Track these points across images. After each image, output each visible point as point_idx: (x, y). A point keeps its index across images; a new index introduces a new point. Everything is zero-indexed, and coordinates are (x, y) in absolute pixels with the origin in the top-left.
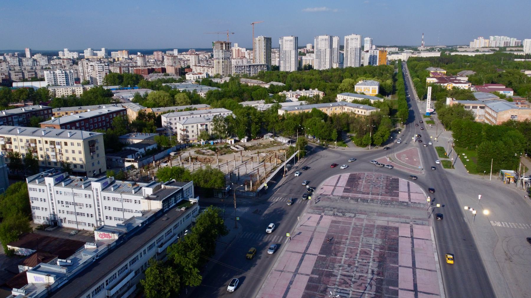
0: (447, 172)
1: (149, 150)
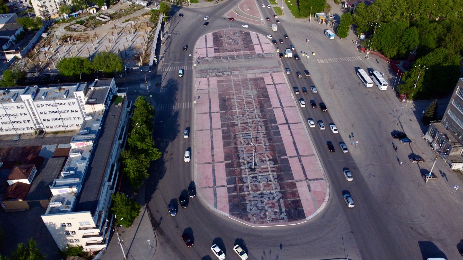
1: (18, 34)
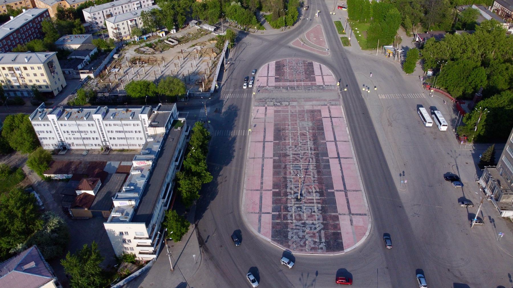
0: (346, 51)
1: (92, 55)
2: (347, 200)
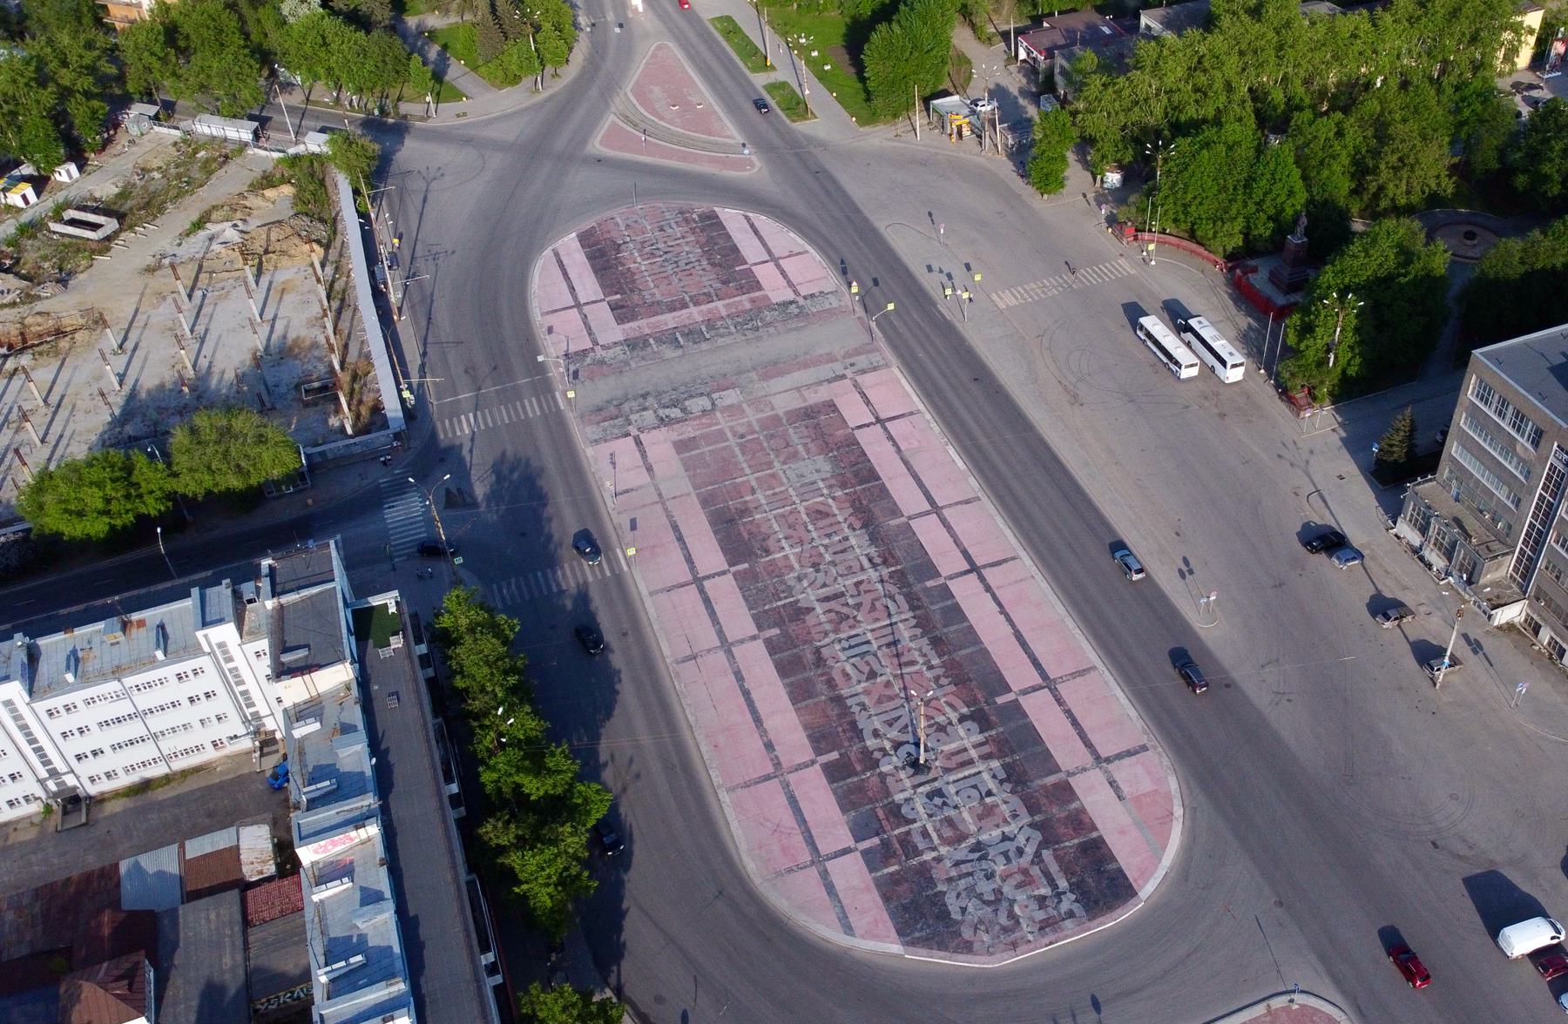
2: (1069, 713)
